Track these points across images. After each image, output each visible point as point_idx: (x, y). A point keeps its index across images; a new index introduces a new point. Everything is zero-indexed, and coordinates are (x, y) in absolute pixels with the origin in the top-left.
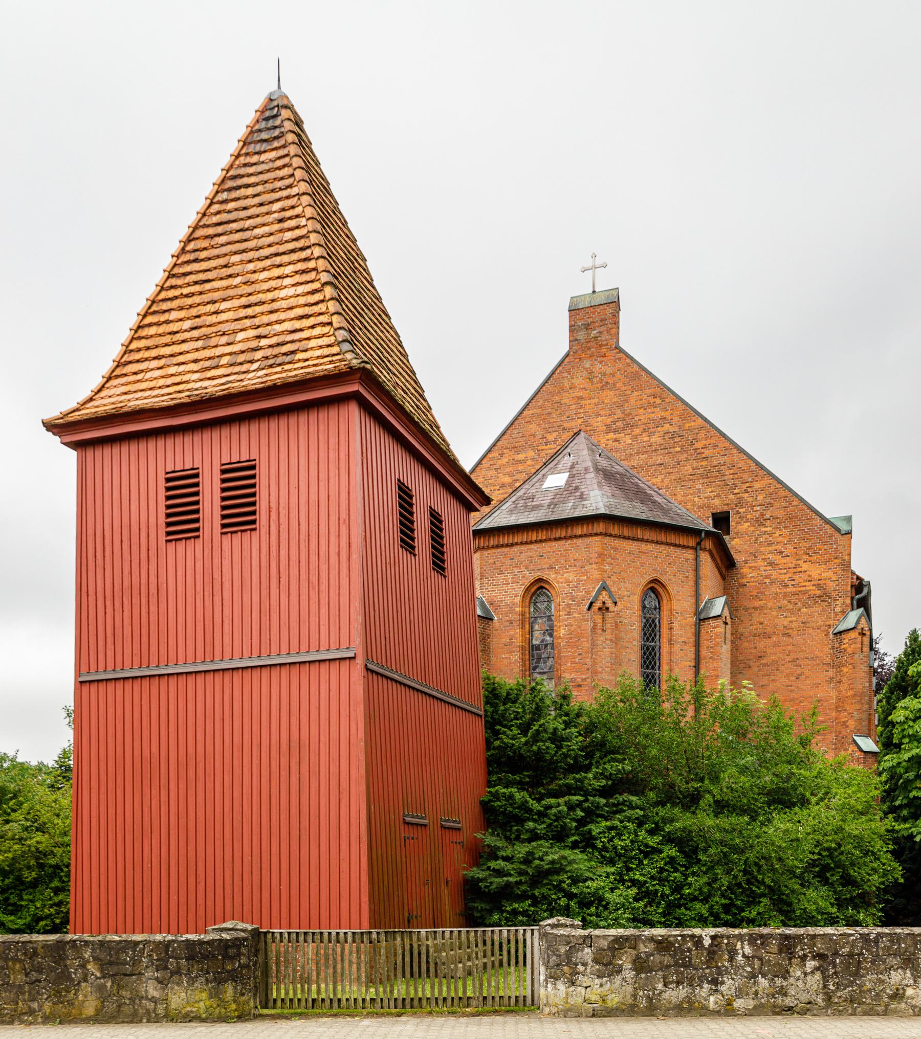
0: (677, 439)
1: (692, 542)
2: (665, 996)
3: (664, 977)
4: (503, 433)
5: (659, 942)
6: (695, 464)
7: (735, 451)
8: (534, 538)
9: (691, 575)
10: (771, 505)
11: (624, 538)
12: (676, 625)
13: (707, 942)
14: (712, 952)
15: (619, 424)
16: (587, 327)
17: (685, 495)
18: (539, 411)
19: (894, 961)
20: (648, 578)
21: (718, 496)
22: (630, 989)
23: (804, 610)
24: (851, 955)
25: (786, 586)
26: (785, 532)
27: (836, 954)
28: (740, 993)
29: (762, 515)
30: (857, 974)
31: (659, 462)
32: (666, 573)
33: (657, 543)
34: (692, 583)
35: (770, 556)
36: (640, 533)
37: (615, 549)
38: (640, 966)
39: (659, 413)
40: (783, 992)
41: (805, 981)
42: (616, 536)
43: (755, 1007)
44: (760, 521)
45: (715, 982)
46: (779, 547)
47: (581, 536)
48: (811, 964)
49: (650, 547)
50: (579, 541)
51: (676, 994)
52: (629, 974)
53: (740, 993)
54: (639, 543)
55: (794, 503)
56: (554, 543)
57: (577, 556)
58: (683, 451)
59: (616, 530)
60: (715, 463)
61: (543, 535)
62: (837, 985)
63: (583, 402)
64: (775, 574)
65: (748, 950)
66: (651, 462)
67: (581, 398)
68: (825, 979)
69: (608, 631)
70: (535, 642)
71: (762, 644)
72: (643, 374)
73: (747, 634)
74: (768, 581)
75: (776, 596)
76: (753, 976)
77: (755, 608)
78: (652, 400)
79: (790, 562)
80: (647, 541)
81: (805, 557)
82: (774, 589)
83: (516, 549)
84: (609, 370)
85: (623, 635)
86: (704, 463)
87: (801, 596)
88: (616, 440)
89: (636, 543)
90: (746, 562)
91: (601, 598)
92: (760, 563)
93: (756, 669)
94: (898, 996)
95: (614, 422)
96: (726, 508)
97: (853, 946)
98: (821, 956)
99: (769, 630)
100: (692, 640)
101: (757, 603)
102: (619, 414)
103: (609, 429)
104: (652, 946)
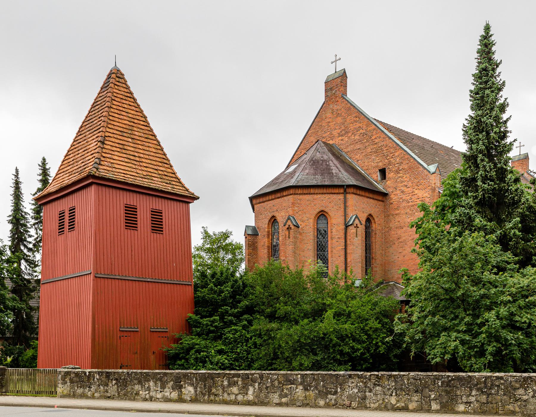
0: (365, 136)
1: (342, 191)
2: (77, 391)
3: (77, 385)
4: (301, 143)
5: (76, 374)
6: (372, 147)
7: (387, 139)
8: (299, 192)
9: (342, 206)
10: (402, 163)
11: (304, 194)
12: (334, 230)
13: (87, 374)
14: (89, 377)
15: (343, 132)
16: (331, 89)
17: (368, 162)
18: (314, 131)
19: (136, 382)
20: (318, 210)
21: (381, 161)
22: (69, 389)
23: (416, 213)
24: (124, 379)
25: (409, 202)
26: (408, 175)
27: (120, 379)
28: (96, 391)
29: (399, 168)
30: (126, 386)
31: (358, 148)
32: (328, 207)
33: (322, 194)
34: (343, 210)
35: (402, 188)
36: (312, 191)
37: (300, 200)
38: (72, 382)
39: (358, 125)
40: (107, 391)
41: (113, 388)
42: (300, 194)
43: (100, 396)
44: (397, 172)
45: (90, 387)
46: (405, 183)
47: (286, 196)
48: (114, 382)
49: (319, 196)
50: (285, 198)
51: (80, 391)
52: (69, 384)
53: (96, 391)
54: (313, 195)
55: (411, 161)
56: (278, 200)
57: (285, 205)
58: (367, 141)
59: (300, 191)
60: (380, 145)
61: (273, 196)
62: (121, 389)
63: (330, 124)
64: (404, 197)
65: (98, 377)
66: (355, 148)
67: (329, 122)
68: (118, 387)
69: (291, 238)
70: (274, 244)
71: (399, 232)
72: (352, 107)
73: (393, 228)
74: (401, 200)
75: (404, 208)
76: (99, 386)
77: (396, 214)
78: (355, 119)
79: (410, 190)
80: (317, 194)
81: (416, 187)
82: (404, 204)
83: (266, 203)
84: (339, 108)
85: (304, 238)
86: (375, 146)
87: (415, 207)
88: (342, 140)
89: (311, 195)
90: (392, 192)
91: (288, 223)
92: (398, 192)
93: (397, 244)
94: (137, 394)
95: (341, 132)
96: (384, 167)
97: (125, 376)
98: (116, 379)
99: (402, 225)
100: (343, 236)
101: (397, 212)
102: (343, 128)
103: (340, 135)
104: (74, 375)
